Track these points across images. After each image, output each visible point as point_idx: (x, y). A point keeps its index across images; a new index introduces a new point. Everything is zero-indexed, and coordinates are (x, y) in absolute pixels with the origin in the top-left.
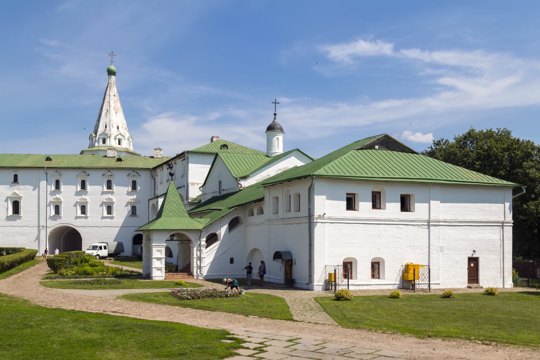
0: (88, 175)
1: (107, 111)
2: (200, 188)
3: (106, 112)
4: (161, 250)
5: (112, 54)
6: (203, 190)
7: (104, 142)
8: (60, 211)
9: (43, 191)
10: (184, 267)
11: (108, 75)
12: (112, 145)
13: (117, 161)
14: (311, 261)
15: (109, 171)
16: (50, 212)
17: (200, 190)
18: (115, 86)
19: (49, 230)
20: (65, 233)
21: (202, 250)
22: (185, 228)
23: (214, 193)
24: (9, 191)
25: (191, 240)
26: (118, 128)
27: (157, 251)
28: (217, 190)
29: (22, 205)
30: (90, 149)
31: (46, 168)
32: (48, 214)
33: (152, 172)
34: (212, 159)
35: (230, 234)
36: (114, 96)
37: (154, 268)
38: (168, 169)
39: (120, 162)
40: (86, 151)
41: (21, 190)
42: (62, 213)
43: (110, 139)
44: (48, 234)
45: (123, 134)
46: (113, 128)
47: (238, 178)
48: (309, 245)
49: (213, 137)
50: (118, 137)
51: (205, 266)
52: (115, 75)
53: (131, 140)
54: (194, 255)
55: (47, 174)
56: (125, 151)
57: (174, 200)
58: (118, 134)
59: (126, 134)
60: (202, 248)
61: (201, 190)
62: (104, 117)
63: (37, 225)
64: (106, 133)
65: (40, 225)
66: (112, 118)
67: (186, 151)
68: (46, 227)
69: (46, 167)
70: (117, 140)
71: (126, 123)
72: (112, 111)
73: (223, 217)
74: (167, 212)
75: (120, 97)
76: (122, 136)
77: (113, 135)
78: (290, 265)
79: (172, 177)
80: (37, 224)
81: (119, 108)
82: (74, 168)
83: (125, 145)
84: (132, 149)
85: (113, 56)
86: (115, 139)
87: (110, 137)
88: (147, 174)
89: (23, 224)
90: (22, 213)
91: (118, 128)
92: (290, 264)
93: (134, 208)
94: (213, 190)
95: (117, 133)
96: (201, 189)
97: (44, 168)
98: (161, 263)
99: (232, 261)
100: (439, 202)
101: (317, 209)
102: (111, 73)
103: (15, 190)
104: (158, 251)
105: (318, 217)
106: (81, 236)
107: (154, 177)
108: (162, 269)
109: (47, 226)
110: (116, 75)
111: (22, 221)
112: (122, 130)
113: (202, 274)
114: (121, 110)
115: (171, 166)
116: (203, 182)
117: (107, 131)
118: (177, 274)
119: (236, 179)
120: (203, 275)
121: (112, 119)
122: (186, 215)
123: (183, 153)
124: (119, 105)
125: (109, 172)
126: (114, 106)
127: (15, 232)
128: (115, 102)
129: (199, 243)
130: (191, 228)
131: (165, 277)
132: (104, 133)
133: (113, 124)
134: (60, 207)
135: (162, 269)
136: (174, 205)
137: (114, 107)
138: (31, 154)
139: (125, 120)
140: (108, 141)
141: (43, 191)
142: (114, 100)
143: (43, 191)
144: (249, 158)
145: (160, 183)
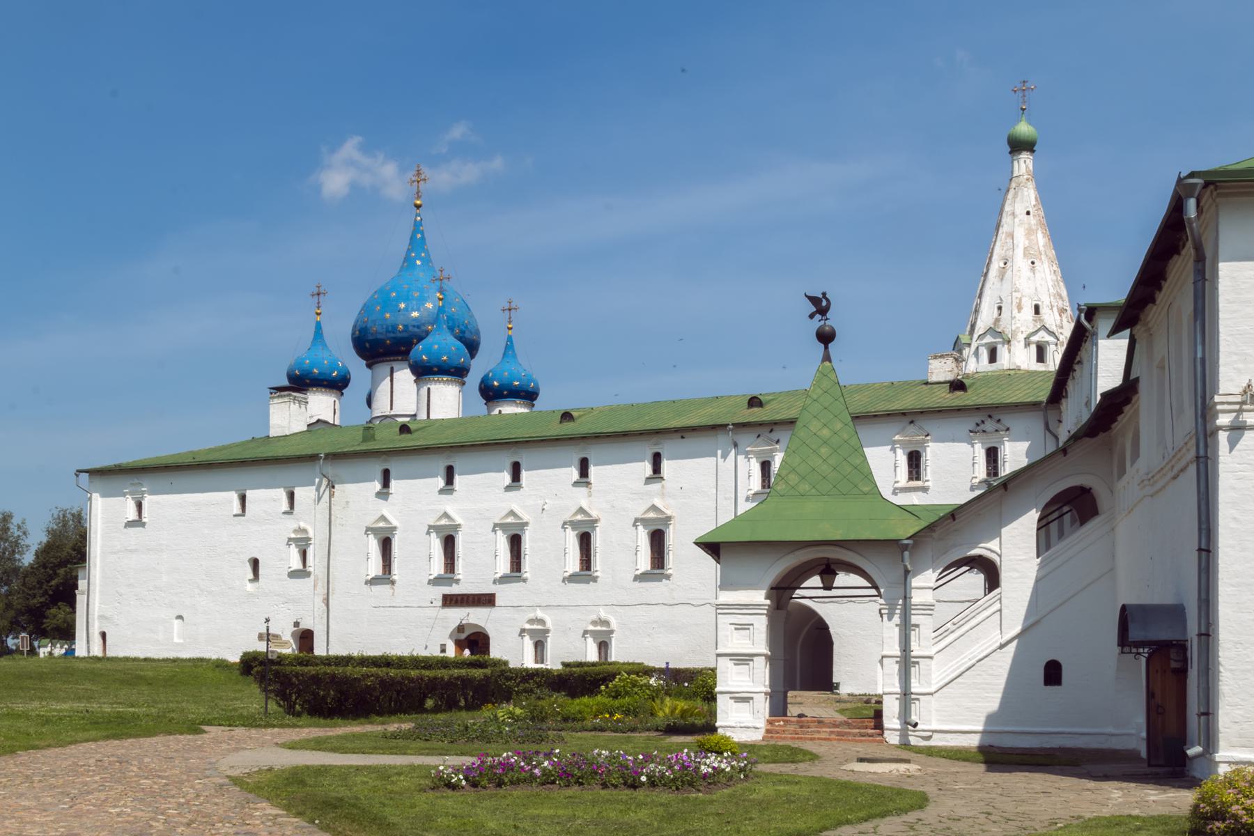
3: (1002, 265)
4: (752, 625)
7: (993, 357)
9: (726, 499)
14: (1208, 635)
15: (912, 422)
18: (1031, 185)
24: (641, 501)
27: (736, 629)
31: (731, 427)
36: (1028, 213)
38: (812, 316)
39: (959, 393)
45: (1053, 328)
46: (1019, 312)
48: (1200, 550)
50: (1034, 339)
51: (932, 689)
58: (1036, 329)
59: (1062, 327)
62: (993, 284)
64: (1000, 331)
69: (733, 424)
70: (1033, 348)
71: (1067, 291)
72: (1021, 263)
77: (1020, 334)
78: (1175, 671)
79: (826, 348)
81: (1042, 248)
86: (1027, 344)
89: (674, 599)
92: (1174, 665)
95: (1032, 326)
101: (1235, 358)
102: (1018, 146)
103: (656, 499)
105: (1239, 399)
106: (832, 630)
108: (752, 698)
110: (1034, 149)
111: (672, 590)
115: (824, 303)
117: (1001, 323)
120: (919, 727)
121: (1018, 285)
124: (1041, 239)
125: (912, 425)
126: (1027, 244)
128: (1030, 232)
132: (991, 331)
133: (1020, 300)
136: (824, 451)
137: (1025, 248)
138: (722, 397)
139: (1062, 284)
140: (1002, 352)
141: (726, 496)
142: (1026, 226)
143: (726, 499)
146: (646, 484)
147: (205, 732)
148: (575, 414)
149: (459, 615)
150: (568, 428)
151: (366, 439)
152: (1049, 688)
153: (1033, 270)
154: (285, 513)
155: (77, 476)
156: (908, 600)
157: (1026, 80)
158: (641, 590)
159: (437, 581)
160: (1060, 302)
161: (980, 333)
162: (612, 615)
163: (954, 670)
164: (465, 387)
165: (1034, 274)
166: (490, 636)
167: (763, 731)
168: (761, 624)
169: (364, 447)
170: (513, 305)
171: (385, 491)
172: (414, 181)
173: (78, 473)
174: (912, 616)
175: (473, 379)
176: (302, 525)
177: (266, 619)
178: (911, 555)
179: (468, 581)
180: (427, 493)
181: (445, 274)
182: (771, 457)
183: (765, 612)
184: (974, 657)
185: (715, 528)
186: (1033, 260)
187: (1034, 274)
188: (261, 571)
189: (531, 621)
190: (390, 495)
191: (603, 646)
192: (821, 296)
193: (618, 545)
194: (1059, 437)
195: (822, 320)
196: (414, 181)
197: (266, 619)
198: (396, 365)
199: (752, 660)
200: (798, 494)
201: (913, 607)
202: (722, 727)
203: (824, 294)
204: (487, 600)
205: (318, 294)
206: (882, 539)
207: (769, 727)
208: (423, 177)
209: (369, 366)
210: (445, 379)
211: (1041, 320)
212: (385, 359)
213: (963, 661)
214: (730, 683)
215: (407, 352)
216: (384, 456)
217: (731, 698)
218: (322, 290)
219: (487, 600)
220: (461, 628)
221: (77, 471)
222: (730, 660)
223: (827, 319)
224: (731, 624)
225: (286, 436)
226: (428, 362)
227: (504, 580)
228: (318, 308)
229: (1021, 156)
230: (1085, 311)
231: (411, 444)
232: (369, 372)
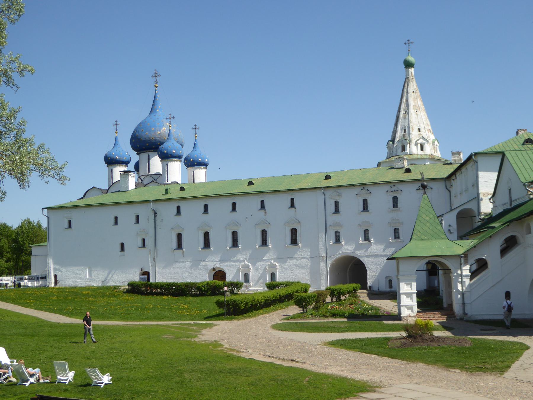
0: (370, 193)
1: (406, 112)
2: (490, 199)
5: (408, 43)
6: (493, 201)
11: (405, 68)
12: (412, 152)
13: (405, 173)
17: (490, 202)
18: (414, 80)
19: (330, 262)
20: (350, 265)
21: (465, 282)
22: (439, 254)
23: (504, 204)
26: (419, 131)
28: (507, 200)
30: (388, 160)
31: (323, 188)
33: (445, 182)
34: (499, 159)
35: (503, 259)
37: (403, 306)
39: (408, 174)
40: (383, 162)
43: (410, 145)
45: (426, 137)
47: (526, 183)
49: (518, 130)
52: (414, 67)
53: (436, 143)
55: (324, 195)
56: (429, 158)
57: (427, 218)
59: (429, 137)
61: (492, 202)
66: (411, 119)
67: (474, 153)
69: (323, 187)
70: (419, 146)
72: (412, 111)
73: (490, 237)
74: (419, 234)
75: (421, 93)
76: (424, 140)
82: (353, 186)
83: (429, 150)
84: (438, 154)
87: (410, 143)
88: (441, 186)
91: (419, 131)
93: (264, 233)
94: (504, 203)
96: (491, 201)
97: (321, 188)
98: (412, 299)
100: (492, 207)
102: (408, 65)
106: (366, 266)
107: (448, 188)
110: (414, 66)
112: (424, 133)
114: (422, 107)
116: (492, 191)
118: (434, 314)
119: (524, 185)
122: (443, 237)
123: (470, 158)
124: (420, 102)
127: (294, 265)
130: (448, 254)
133: (413, 126)
136: (428, 224)
139: (428, 119)
144: (520, 156)
145: (454, 196)
147: (215, 325)
153: (417, 114)
155: (43, 210)
157: (409, 39)
160: (428, 127)
165: (417, 116)
172: (154, 77)
173: (43, 209)
181: (172, 116)
186: (416, 110)
187: (417, 116)
194: (451, 191)
196: (154, 77)
198: (151, 154)
200: (421, 239)
205: (116, 125)
208: (158, 75)
209: (138, 154)
211: (421, 134)
212: (146, 151)
214: (405, 302)
216: (178, 201)
218: (118, 123)
221: (43, 208)
228: (116, 130)
229: (409, 69)
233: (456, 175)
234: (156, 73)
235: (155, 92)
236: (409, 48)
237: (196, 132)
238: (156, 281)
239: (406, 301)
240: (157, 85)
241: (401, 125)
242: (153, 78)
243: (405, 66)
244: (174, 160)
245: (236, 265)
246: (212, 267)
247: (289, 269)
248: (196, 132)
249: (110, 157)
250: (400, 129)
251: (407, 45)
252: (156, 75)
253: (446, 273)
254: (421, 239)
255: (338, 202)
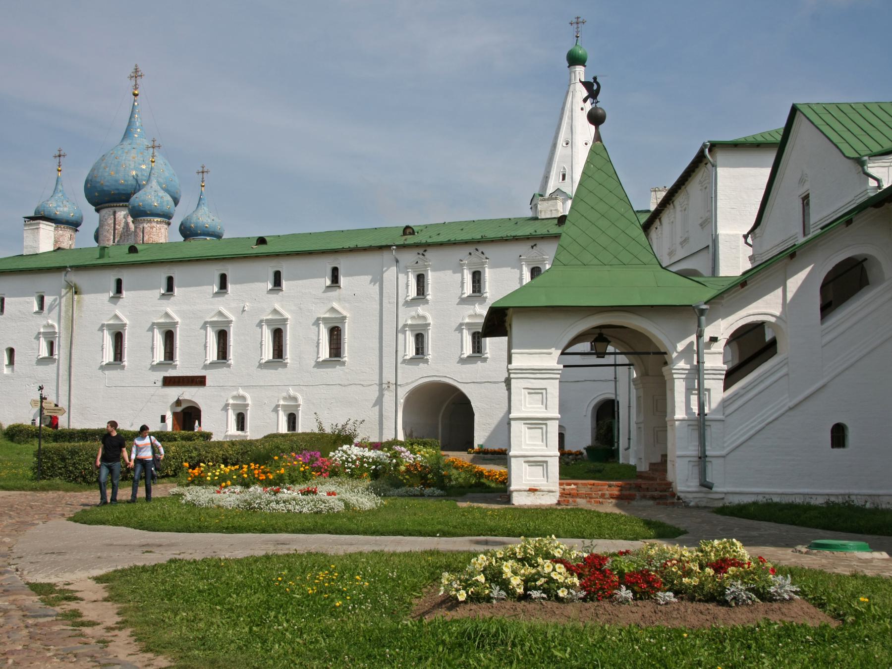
1: (567, 144)
2: (746, 237)
4: (546, 389)
8: (425, 345)
10: (651, 465)
16: (405, 351)
17: (746, 243)
19: (403, 393)
21: (709, 390)
25: (665, 353)
27: (529, 393)
29: (346, 337)
32: (400, 354)
41: (345, 301)
42: (430, 352)
44: (401, 401)
51: (724, 453)
54: (677, 410)
60: (707, 384)
63: (377, 382)
65: (383, 382)
67: (709, 142)
68: (396, 384)
79: (597, 129)
80: (378, 380)
85: (580, 25)
90: (346, 354)
96: (749, 240)
98: (545, 438)
99: (839, 435)
104: (533, 391)
108: (546, 462)
109: (399, 383)
111: (347, 373)
113: (711, 488)
115: (595, 87)
127: (333, 398)
129: (695, 363)
131: (562, 495)
134: (426, 337)
135: (546, 462)
146: (325, 292)
148: (267, 239)
149: (175, 393)
150: (263, 249)
151: (102, 256)
152: (836, 450)
154: (36, 313)
156: (701, 364)
158: (322, 373)
159: (155, 368)
161: (551, 192)
162: (299, 393)
163: (744, 434)
164: (170, 226)
166: (202, 409)
167: (558, 494)
168: (553, 388)
169: (101, 261)
170: (205, 169)
171: (118, 295)
172: (132, 77)
174: (705, 381)
175: (176, 222)
176: (50, 322)
177: (40, 387)
178: (707, 319)
179: (181, 368)
180: (151, 298)
181: (156, 144)
182: (425, 271)
183: (723, 377)
184: (763, 421)
185: (518, 287)
188: (16, 358)
189: (234, 398)
190: (121, 300)
191: (292, 420)
192: (592, 81)
193: (304, 338)
195: (593, 103)
196: (132, 77)
197: (40, 387)
199: (546, 424)
201: (705, 372)
202: (516, 491)
203: (595, 79)
204: (199, 381)
206: (678, 304)
207: (563, 491)
208: (140, 74)
209: (97, 211)
210: (155, 220)
213: (753, 425)
215: (127, 200)
217: (525, 462)
218: (62, 153)
219: (199, 381)
220: (178, 402)
222: (524, 424)
223: (598, 102)
224: (524, 388)
225: (37, 254)
226: (143, 207)
227: (213, 364)
228: (59, 166)
230: (709, 146)
231: (139, 259)
232: (97, 215)
233: (662, 219)
234: (136, 70)
235: (134, 104)
236: (577, 32)
237: (203, 178)
238: (69, 425)
239: (528, 445)
240: (136, 92)
241: (557, 167)
242: (130, 79)
243: (569, 63)
244: (155, 220)
245: (221, 396)
246: (175, 400)
247: (322, 406)
248: (203, 178)
249: (44, 212)
250: (556, 174)
251: (575, 26)
252: (136, 74)
253: (647, 375)
254: (580, 263)
255: (424, 277)
